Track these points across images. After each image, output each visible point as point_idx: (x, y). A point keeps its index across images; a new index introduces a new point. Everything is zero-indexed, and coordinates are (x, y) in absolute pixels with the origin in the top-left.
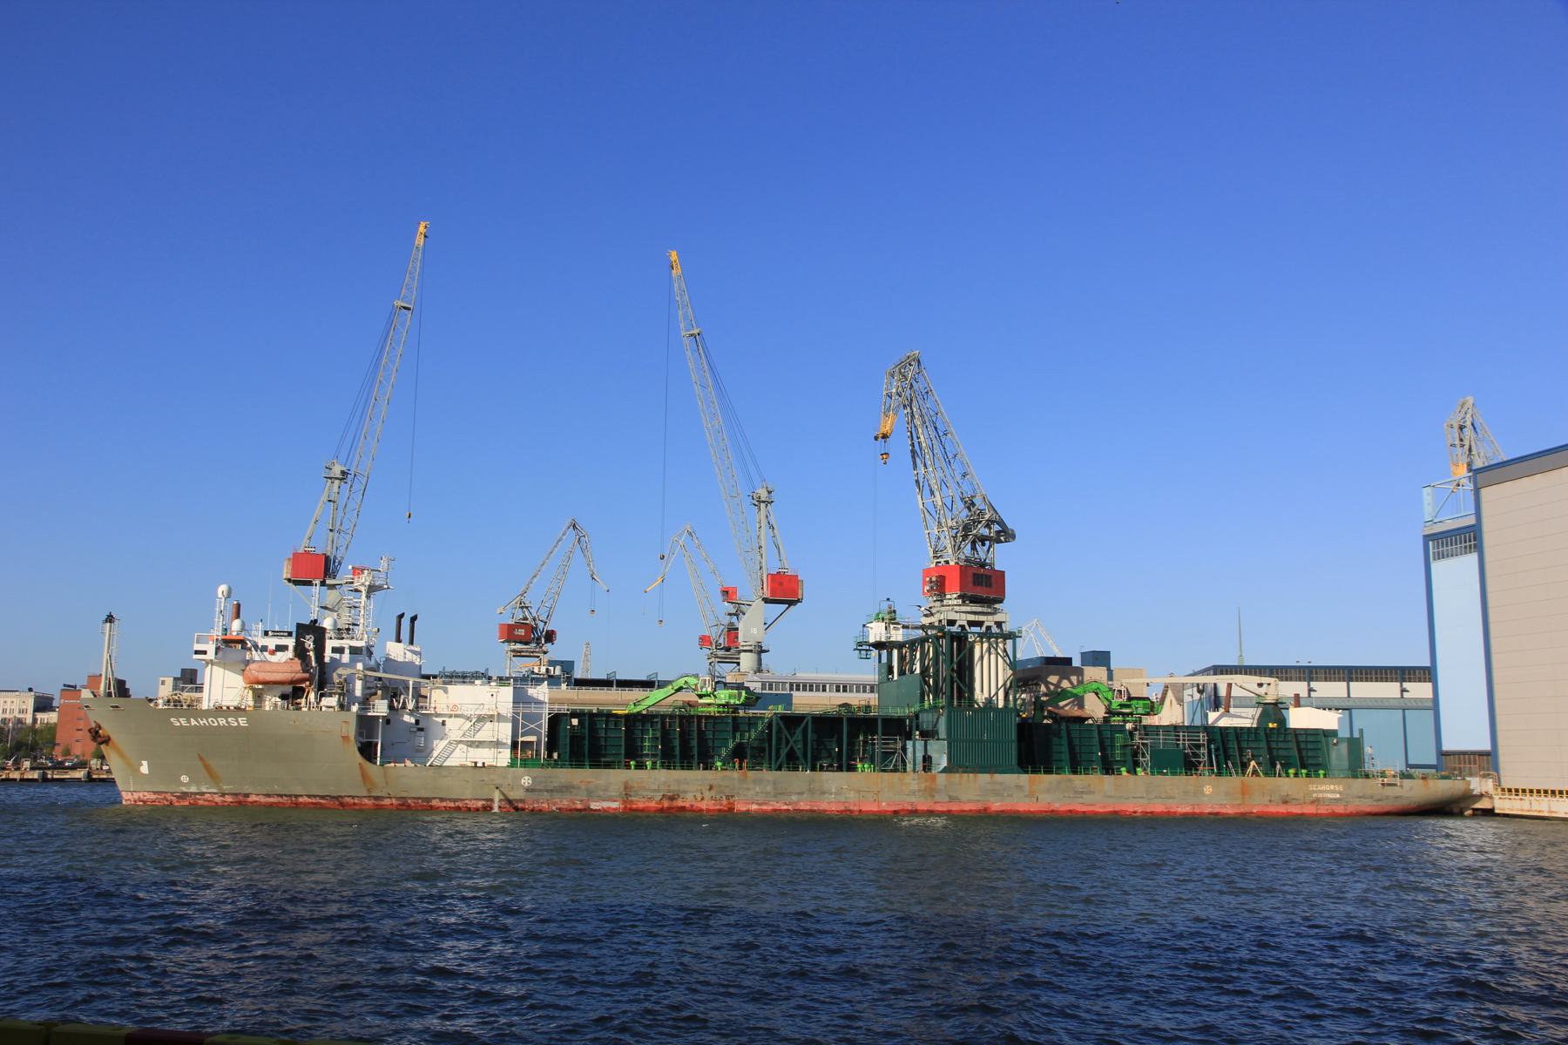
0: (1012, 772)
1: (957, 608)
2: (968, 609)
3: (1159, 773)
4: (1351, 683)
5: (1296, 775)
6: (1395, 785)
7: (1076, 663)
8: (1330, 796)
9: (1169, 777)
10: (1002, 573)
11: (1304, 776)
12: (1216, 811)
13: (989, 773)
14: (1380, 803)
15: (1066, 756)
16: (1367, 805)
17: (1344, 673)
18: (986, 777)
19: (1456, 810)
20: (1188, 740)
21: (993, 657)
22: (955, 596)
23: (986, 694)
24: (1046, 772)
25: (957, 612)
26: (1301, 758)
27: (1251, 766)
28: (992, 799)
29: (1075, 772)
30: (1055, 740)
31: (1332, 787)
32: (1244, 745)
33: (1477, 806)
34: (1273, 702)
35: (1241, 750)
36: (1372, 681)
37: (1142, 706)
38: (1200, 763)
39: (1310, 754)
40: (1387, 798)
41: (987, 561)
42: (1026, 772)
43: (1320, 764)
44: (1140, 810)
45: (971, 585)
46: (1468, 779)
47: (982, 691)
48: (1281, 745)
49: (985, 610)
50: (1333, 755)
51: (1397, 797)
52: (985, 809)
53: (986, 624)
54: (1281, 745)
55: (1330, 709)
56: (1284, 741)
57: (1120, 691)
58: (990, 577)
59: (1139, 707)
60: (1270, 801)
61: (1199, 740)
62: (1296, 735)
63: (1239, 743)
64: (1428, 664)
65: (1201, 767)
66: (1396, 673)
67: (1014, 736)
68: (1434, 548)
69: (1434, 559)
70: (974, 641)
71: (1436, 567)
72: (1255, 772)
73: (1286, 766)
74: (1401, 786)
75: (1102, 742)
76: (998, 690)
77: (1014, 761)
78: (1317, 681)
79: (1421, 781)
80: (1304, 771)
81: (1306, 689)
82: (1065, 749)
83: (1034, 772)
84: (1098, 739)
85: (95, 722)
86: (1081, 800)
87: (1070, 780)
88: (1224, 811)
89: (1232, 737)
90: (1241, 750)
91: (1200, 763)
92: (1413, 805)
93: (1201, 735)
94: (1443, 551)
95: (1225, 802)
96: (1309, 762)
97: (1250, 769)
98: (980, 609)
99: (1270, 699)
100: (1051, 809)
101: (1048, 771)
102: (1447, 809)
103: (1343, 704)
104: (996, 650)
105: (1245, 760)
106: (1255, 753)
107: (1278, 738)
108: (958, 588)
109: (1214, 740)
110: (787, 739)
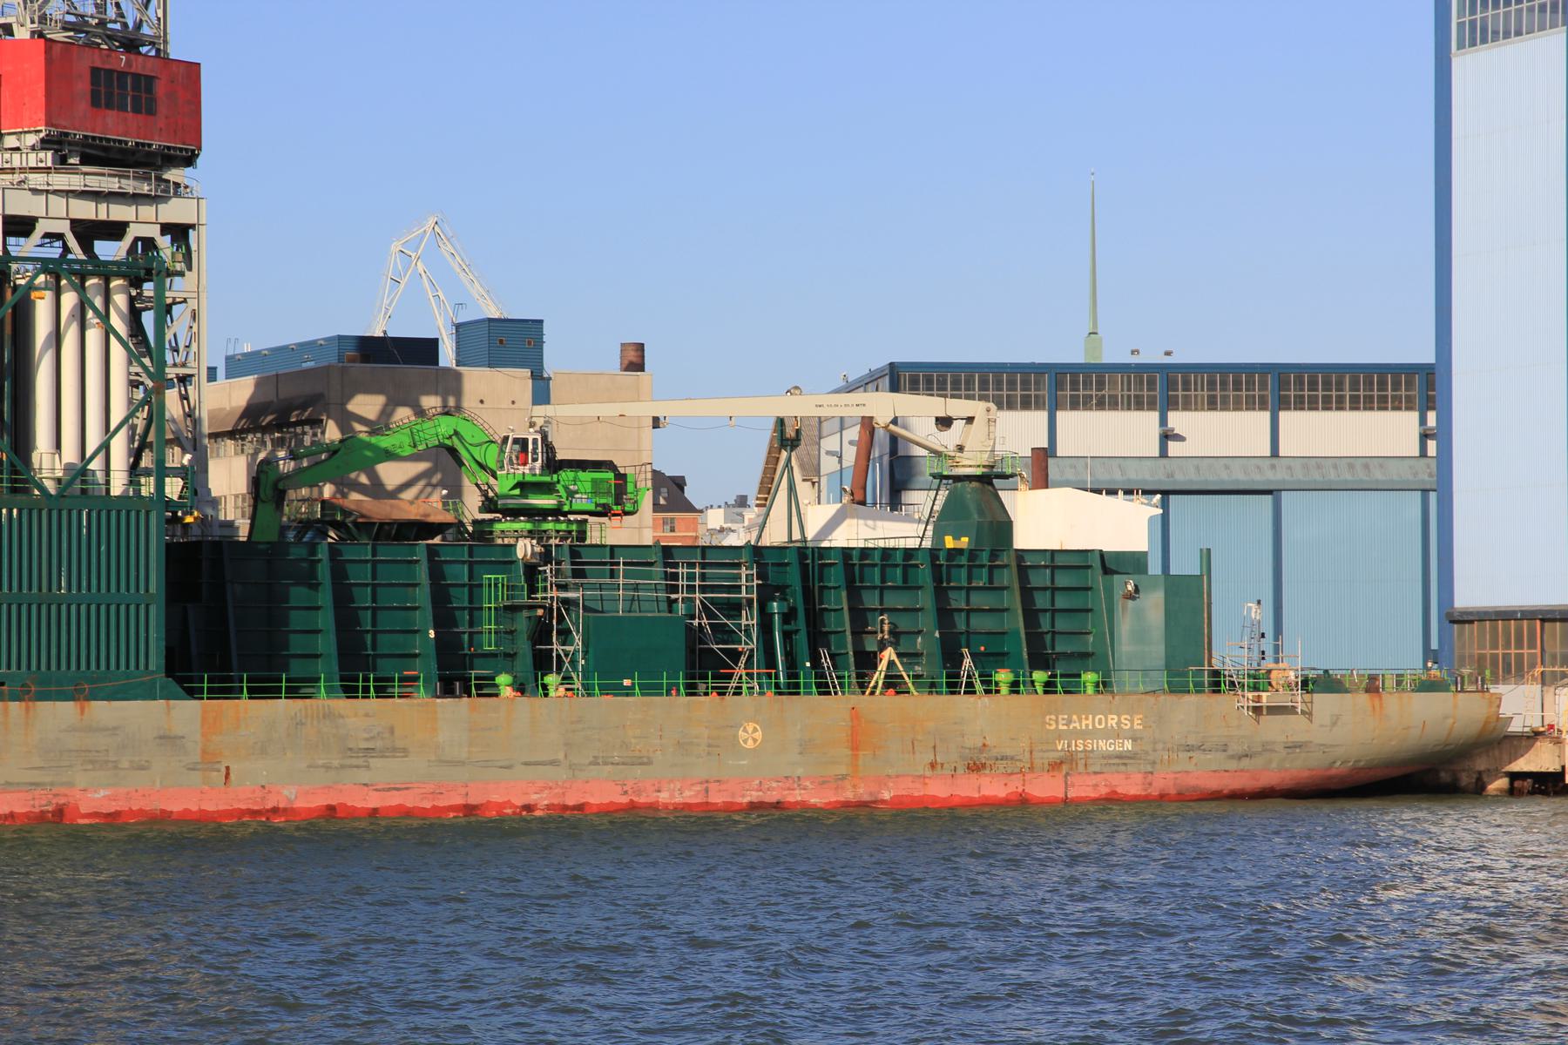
0: (150, 695)
1: (37, 180)
2: (75, 182)
3: (606, 690)
4: (1283, 415)
5: (1014, 687)
6: (1291, 710)
7: (447, 355)
8: (1104, 746)
9: (637, 700)
10: (192, 71)
11: (1040, 689)
12: (772, 797)
13: (73, 699)
14: (1245, 763)
15: (326, 643)
16: (1207, 772)
17: (1263, 386)
18: (62, 712)
19: (1465, 780)
20: (703, 589)
21: (93, 336)
22: (31, 139)
23: (70, 454)
24: (255, 693)
25: (35, 191)
26: (1035, 638)
27: (883, 666)
28: (81, 780)
29: (350, 691)
30: (298, 594)
31: (1113, 721)
32: (871, 600)
33: (1522, 765)
34: (979, 472)
35: (860, 618)
36: (1340, 408)
37: (588, 486)
38: (735, 656)
39: (1062, 624)
40: (1267, 748)
41: (146, 30)
42: (193, 693)
43: (1004, 654)
44: (542, 799)
45: (83, 106)
46: (1494, 689)
47: (58, 445)
48: (978, 600)
49: (130, 186)
50: (1125, 626)
51: (1292, 747)
52: (60, 812)
53: (133, 232)
54: (978, 600)
55: (1128, 492)
56: (991, 588)
57: (523, 443)
58: (150, 79)
59: (582, 490)
60: (933, 765)
61: (738, 589)
62: (1023, 571)
63: (854, 592)
64: (1428, 357)
65: (740, 670)
66: (1151, 384)
67: (155, 583)
68: (1461, 14)
69: (1461, 46)
70: (30, 287)
71: (1465, 65)
72: (893, 683)
73: (989, 660)
74: (1308, 714)
75: (440, 595)
76: (108, 432)
77: (156, 660)
78: (1187, 408)
79: (1363, 699)
80: (1040, 676)
81: (1155, 431)
82: (325, 620)
83: (216, 693)
84: (427, 590)
85: (1207, 555)
86: (364, 776)
87: (329, 715)
88: (796, 796)
89: (835, 577)
90: (860, 618)
91: (735, 656)
92: (1339, 768)
93: (744, 572)
94: (1484, 20)
95: (800, 771)
96: (1058, 649)
97: (878, 677)
98: (112, 184)
99: (970, 464)
100: (269, 806)
101: (263, 690)
102: (1445, 777)
103: (1258, 477)
104: (105, 317)
105: (871, 646)
106: (904, 624)
107: (970, 580)
108: (42, 115)
109: (782, 589)
110: (714, 617)
